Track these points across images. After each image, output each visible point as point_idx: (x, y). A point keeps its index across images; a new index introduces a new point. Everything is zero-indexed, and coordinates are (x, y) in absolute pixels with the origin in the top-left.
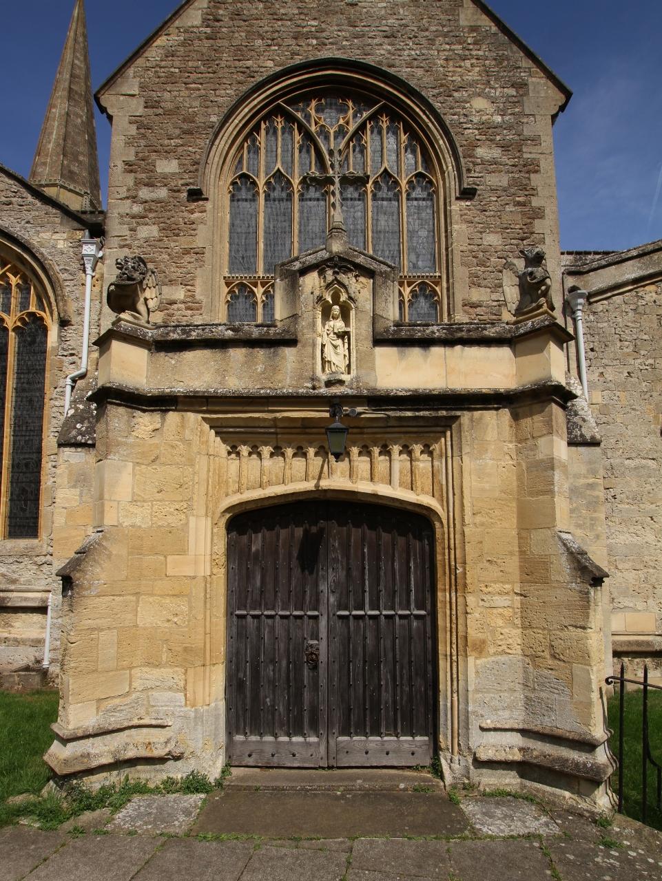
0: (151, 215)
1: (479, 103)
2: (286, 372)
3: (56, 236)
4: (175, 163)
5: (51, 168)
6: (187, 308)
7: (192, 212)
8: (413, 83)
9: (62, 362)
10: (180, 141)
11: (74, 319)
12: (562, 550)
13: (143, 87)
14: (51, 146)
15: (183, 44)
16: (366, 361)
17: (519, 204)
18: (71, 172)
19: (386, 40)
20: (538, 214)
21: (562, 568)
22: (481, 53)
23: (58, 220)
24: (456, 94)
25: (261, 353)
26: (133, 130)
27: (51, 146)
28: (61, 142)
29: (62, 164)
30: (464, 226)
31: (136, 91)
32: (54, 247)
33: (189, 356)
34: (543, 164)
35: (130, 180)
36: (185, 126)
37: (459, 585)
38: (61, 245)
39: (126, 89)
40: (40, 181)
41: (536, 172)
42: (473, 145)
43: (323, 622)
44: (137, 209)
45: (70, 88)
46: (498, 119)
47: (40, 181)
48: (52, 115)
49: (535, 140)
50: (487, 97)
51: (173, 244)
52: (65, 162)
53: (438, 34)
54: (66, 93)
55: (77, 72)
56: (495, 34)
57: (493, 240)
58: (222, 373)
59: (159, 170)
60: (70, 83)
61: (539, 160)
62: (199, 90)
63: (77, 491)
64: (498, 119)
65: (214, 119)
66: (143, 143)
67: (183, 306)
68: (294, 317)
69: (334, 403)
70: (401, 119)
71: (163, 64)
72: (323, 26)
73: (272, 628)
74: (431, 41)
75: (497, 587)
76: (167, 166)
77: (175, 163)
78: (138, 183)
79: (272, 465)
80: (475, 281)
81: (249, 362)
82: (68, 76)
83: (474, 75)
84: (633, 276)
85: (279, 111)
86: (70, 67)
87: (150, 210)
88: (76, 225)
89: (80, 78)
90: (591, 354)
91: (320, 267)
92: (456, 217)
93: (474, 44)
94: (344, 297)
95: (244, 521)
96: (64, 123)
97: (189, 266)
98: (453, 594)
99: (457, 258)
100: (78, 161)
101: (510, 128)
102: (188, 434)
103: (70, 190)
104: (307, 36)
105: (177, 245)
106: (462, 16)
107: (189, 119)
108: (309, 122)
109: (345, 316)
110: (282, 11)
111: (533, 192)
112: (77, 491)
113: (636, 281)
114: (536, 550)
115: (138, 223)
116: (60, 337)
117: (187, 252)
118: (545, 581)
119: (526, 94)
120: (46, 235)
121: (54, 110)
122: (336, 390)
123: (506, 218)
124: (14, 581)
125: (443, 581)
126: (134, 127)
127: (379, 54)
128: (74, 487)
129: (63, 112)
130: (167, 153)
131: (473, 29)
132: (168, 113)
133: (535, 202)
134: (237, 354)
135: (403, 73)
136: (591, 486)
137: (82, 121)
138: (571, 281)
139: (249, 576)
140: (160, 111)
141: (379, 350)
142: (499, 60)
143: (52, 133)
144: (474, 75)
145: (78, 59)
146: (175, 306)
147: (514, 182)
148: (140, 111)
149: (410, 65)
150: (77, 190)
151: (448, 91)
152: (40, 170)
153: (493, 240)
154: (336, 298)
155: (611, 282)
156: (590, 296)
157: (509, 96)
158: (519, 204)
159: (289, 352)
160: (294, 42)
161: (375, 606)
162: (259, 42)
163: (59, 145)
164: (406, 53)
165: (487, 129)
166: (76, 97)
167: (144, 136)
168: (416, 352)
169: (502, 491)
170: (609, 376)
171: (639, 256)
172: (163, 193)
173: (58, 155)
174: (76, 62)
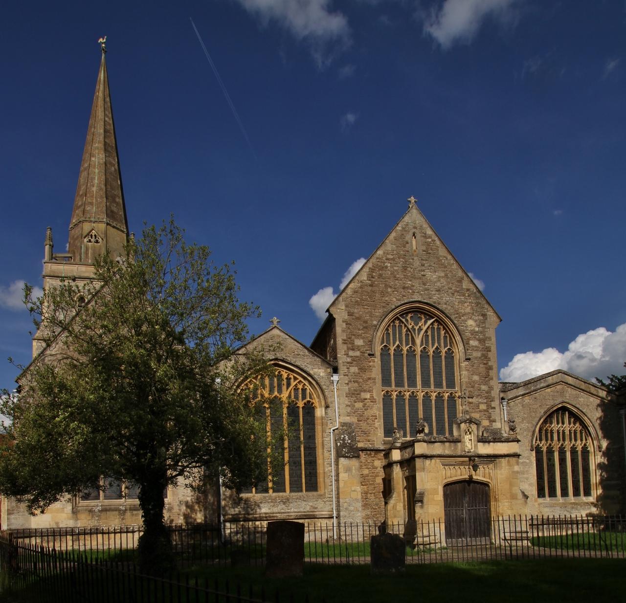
0: (354, 363)
1: (470, 322)
2: (459, 449)
3: (320, 371)
4: (362, 341)
5: (98, 208)
6: (371, 402)
7: (370, 362)
8: (446, 312)
9: (327, 423)
10: (363, 331)
11: (331, 405)
12: (520, 491)
13: (347, 306)
14: (94, 189)
15: (361, 287)
16: (476, 446)
17: (484, 364)
18: (112, 212)
19: (437, 293)
20: (491, 368)
21: (520, 496)
22: (470, 300)
23: (320, 363)
24: (462, 318)
25: (452, 444)
26: (344, 325)
27: (94, 189)
28: (103, 187)
29: (106, 205)
30: (466, 372)
31: (343, 307)
32: (319, 375)
33: (436, 444)
34: (492, 348)
35: (345, 347)
36: (364, 325)
37: (496, 500)
38: (322, 374)
39: (339, 307)
40: (90, 218)
41: (490, 351)
42: (469, 339)
43: (464, 510)
44: (349, 360)
45: (105, 142)
48: (92, 163)
49: (490, 339)
50: (473, 319)
51: (364, 375)
52: (108, 204)
54: (101, 146)
55: (108, 127)
56: (475, 293)
57: (476, 378)
58: (444, 450)
59: (356, 344)
60: (105, 137)
61: (490, 346)
62: (368, 309)
63: (347, 474)
64: (477, 329)
65: (375, 323)
66: (349, 331)
67: (369, 401)
68: (460, 435)
69: (470, 457)
70: (441, 325)
71: (354, 296)
72: (414, 284)
73: (453, 513)
74: (453, 294)
75: (505, 500)
76: (359, 342)
77: (362, 341)
78: (348, 349)
79: (453, 471)
81: (450, 446)
82: (102, 131)
83: (468, 310)
84: (522, 393)
85: (398, 319)
87: (354, 361)
88: (327, 366)
89: (110, 133)
91: (465, 422)
93: (469, 296)
94: (470, 430)
96: (103, 171)
97: (371, 385)
98: (69, 566)
100: (115, 202)
101: (481, 333)
102: (437, 465)
103: (114, 227)
104: (408, 288)
105: (365, 376)
106: (464, 284)
107: (366, 322)
108: (408, 323)
109: (470, 433)
110: (397, 276)
111: (489, 359)
112: (347, 474)
114: (514, 492)
115: (350, 366)
116: (326, 413)
117: (369, 379)
118: (517, 499)
119: (486, 319)
120: (316, 370)
121: (93, 159)
122: (470, 454)
124: (316, 508)
125: (492, 500)
126: (344, 324)
127: (435, 299)
128: (346, 472)
130: (358, 336)
131: (468, 290)
132: (358, 318)
133: (490, 363)
134: (447, 444)
135: (443, 307)
137: (115, 169)
138: (502, 395)
139: (447, 500)
140: (354, 317)
141: (479, 444)
142: (478, 304)
143: (95, 178)
144: (468, 310)
145: (108, 117)
146: (367, 401)
147: (483, 355)
148: (346, 317)
149: (446, 304)
150: (118, 227)
151: (460, 315)
152: (88, 208)
154: (469, 430)
156: (509, 400)
158: (484, 364)
159: (459, 444)
160: (402, 290)
161: (476, 507)
162: (389, 290)
163: (101, 189)
164: (444, 299)
165: (473, 333)
166: (109, 149)
167: (349, 328)
168: (487, 444)
172: (358, 353)
173: (101, 197)
174: (107, 119)
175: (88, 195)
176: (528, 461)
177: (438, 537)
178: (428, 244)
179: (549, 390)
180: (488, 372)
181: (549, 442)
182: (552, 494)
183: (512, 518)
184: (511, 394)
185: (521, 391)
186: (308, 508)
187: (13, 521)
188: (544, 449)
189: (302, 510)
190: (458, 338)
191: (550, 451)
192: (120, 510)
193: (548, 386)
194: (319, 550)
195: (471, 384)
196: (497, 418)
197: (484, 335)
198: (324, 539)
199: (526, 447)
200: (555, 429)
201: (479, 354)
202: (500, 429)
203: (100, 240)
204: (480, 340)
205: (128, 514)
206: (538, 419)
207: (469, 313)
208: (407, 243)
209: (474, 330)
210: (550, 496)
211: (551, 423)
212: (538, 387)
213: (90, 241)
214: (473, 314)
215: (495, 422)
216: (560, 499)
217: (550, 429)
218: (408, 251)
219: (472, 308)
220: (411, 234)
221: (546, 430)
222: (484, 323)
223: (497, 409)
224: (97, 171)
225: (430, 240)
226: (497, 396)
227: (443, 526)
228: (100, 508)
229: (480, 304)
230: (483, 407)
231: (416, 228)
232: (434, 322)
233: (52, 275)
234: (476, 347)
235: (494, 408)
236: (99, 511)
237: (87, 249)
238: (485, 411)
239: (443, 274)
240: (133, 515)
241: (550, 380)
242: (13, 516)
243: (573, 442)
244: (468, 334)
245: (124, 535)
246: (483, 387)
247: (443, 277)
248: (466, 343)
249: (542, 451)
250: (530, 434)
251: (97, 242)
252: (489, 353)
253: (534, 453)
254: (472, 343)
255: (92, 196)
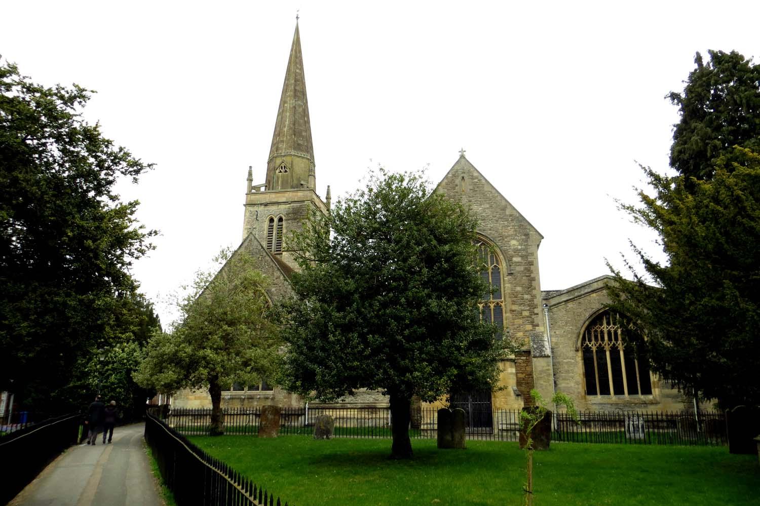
1: (513, 242)
14: (285, 129)
17: (527, 276)
18: (298, 144)
27: (285, 129)
28: (292, 126)
40: (281, 153)
41: (533, 265)
46: (520, 247)
47: (281, 153)
50: (516, 239)
53: (500, 218)
57: (519, 289)
60: (295, 85)
64: (520, 247)
74: (497, 221)
80: (514, 303)
82: (293, 81)
83: (511, 232)
86: (294, 75)
90: (551, 326)
92: (506, 282)
93: (512, 220)
95: (658, 443)
99: (507, 296)
101: (524, 250)
113: (565, 301)
119: (529, 238)
121: (286, 105)
123: (523, 281)
124: (378, 400)
129: (292, 106)
131: (511, 215)
136: (548, 370)
138: (544, 302)
144: (511, 232)
147: (526, 269)
149: (490, 230)
151: (502, 237)
152: (280, 146)
153: (519, 289)
155: (558, 302)
156: (550, 307)
157: (523, 239)
158: (527, 276)
165: (516, 251)
166: (299, 94)
169: (230, 467)
170: (557, 333)
171: (567, 293)
175: (281, 135)
176: (573, 361)
177: (310, 413)
178: (475, 184)
179: (594, 295)
180: (531, 283)
181: (600, 342)
182: (605, 391)
183: (508, 411)
184: (553, 302)
185: (564, 298)
186: (371, 400)
187: (177, 404)
188: (594, 349)
189: (367, 402)
190: (501, 257)
191: (601, 351)
192: (241, 399)
193: (593, 291)
194: (356, 431)
195: (515, 295)
196: (539, 323)
197: (527, 252)
198: (381, 425)
199: (570, 347)
200: (605, 330)
201: (522, 268)
202: (543, 333)
203: (288, 170)
204: (522, 257)
205: (246, 401)
206: (583, 322)
207: (512, 235)
208: (457, 186)
209: (517, 248)
210: (601, 394)
211: (601, 325)
212: (583, 293)
213: (281, 172)
214: (516, 235)
215: (538, 326)
216: (613, 397)
217: (599, 330)
218: (457, 192)
219: (515, 231)
220: (460, 178)
221: (596, 331)
222: (527, 241)
223: (540, 315)
224: (288, 114)
225: (476, 180)
226: (539, 304)
227: (495, 420)
228: (229, 397)
229: (523, 226)
230: (526, 313)
231: (464, 173)
232: (481, 245)
233: (251, 203)
234: (518, 262)
235: (537, 314)
236: (229, 399)
237: (278, 178)
238: (528, 317)
239: (488, 206)
240: (249, 402)
241: (595, 286)
242: (177, 401)
243: (600, 342)
244: (511, 252)
245: (245, 416)
246: (526, 296)
247: (488, 208)
248: (509, 260)
249: (592, 351)
250: (575, 336)
251: (286, 171)
252: (531, 266)
253: (580, 354)
254: (515, 259)
255: (284, 135)
